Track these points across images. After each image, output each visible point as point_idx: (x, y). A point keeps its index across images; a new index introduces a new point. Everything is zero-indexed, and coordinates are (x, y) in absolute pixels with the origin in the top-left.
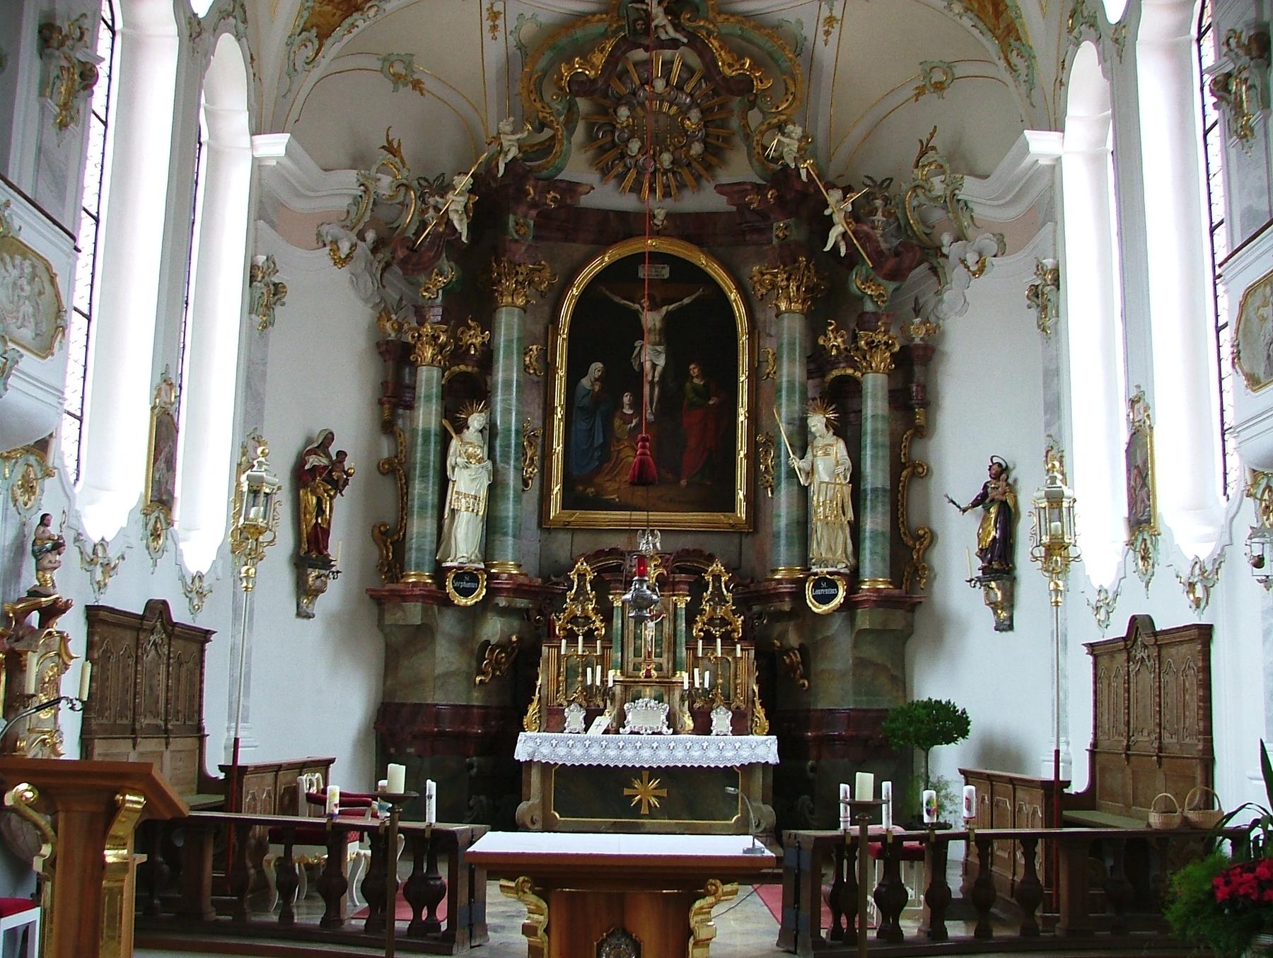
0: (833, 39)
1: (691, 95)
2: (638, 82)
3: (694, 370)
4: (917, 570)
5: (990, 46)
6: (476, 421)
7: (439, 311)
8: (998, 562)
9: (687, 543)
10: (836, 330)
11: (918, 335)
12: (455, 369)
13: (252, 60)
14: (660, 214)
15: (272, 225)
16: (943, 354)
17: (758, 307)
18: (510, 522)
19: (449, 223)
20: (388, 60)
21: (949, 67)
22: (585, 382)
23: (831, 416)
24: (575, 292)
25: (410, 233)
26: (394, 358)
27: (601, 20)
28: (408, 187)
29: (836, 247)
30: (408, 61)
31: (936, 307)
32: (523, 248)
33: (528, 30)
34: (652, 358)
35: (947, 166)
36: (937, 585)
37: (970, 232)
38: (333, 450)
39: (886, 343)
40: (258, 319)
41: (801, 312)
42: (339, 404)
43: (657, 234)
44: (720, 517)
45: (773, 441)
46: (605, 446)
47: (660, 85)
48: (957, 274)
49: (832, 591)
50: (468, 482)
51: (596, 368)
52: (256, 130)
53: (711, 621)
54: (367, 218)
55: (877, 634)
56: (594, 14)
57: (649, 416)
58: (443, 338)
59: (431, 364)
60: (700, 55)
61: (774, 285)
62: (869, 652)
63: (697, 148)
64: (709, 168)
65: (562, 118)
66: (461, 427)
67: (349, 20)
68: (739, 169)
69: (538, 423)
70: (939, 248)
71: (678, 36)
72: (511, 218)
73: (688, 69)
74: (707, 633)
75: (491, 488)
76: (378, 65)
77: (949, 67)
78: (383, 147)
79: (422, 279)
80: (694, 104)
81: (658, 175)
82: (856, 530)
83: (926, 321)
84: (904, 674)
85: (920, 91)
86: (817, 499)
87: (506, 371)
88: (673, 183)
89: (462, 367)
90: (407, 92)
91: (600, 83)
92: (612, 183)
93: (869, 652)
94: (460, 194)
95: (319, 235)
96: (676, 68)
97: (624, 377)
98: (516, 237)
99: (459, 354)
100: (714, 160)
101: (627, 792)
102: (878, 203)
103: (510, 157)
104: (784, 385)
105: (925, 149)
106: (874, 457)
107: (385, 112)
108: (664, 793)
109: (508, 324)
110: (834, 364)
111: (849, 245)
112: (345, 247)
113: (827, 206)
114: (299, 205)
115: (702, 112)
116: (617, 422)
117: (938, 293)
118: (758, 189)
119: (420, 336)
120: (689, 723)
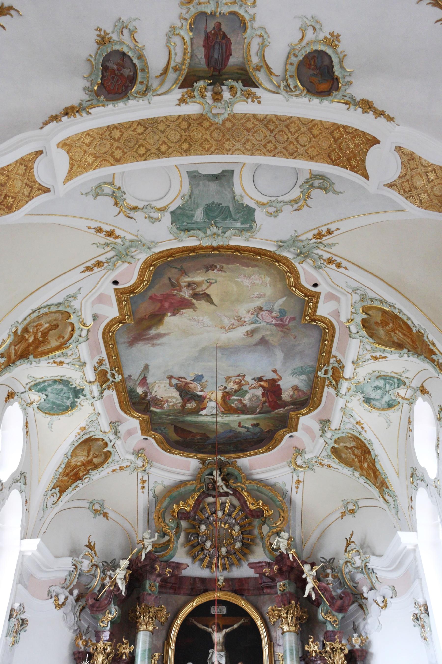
0: (300, 490)
1: (235, 519)
2: (210, 513)
5: (375, 492)
10: (314, 642)
11: (357, 643)
14: (221, 579)
15: (25, 586)
16: (372, 654)
17: (272, 629)
19: (116, 585)
20: (92, 503)
21: (356, 503)
24: (179, 622)
25: (96, 591)
27: (193, 484)
31: (364, 626)
32: (153, 598)
33: (159, 489)
35: (361, 551)
37: (377, 585)
39: (341, 648)
40: (10, 640)
41: (295, 632)
43: (220, 590)
47: (220, 514)
48: (373, 609)
54: (75, 583)
56: (189, 481)
58: (109, 650)
60: (239, 500)
61: (280, 617)
63: (238, 545)
64: (245, 555)
65: (174, 531)
67: (75, 484)
68: (259, 555)
70: (362, 594)
71: (228, 491)
72: (148, 583)
73: (234, 507)
76: (87, 505)
77: (356, 503)
78: (86, 546)
80: (236, 523)
81: (220, 559)
85: (343, 514)
88: (227, 563)
91: (192, 513)
92: (197, 563)
94: (123, 570)
95: (49, 592)
96: (228, 505)
98: (150, 592)
100: (246, 551)
102: (329, 571)
103: (148, 550)
107: (90, 529)
109: (143, 640)
111: (317, 594)
112: (62, 599)
113: (303, 573)
114: (41, 576)
115: (240, 527)
117: (364, 619)
118: (269, 565)
119: (97, 648)
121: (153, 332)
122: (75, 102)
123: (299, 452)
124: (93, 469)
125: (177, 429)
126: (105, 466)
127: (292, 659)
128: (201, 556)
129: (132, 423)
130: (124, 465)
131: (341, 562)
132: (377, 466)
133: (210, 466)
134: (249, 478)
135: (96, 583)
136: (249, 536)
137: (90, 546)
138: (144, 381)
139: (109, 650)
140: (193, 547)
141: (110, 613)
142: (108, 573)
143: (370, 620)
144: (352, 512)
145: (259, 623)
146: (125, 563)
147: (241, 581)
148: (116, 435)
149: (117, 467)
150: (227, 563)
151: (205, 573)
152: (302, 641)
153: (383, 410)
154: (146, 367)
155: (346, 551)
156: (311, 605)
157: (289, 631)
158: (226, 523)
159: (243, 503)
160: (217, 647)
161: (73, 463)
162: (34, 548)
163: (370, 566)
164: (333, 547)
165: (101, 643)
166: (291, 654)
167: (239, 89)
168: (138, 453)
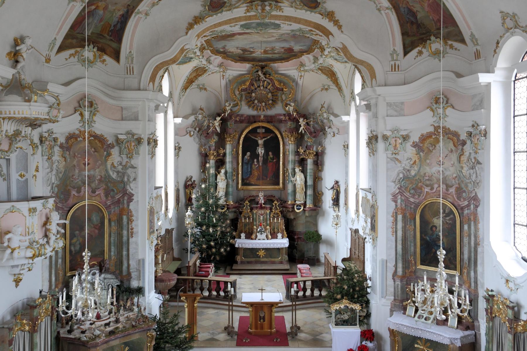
3: (270, 153)
5: (337, 89)
6: (223, 171)
8: (336, 202)
9: (269, 193)
13: (173, 105)
14: (262, 116)
19: (216, 129)
21: (329, 86)
22: (246, 157)
24: (243, 136)
25: (206, 128)
26: (204, 157)
28: (205, 117)
29: (302, 131)
30: (203, 85)
33: (231, 77)
34: (261, 151)
36: (323, 204)
37: (332, 126)
38: (192, 180)
40: (176, 157)
42: (193, 170)
44: (277, 187)
45: (287, 169)
46: (251, 171)
48: (329, 136)
50: (222, 185)
51: (248, 154)
52: (174, 117)
53: (274, 213)
55: (310, 216)
57: (260, 164)
62: (309, 219)
63: (270, 102)
69: (236, 166)
70: (325, 129)
72: (229, 123)
75: (227, 185)
77: (329, 86)
82: (306, 193)
83: (322, 146)
85: (322, 90)
87: (228, 159)
90: (203, 91)
93: (309, 219)
99: (218, 155)
100: (274, 103)
105: (322, 107)
109: (228, 148)
110: (301, 155)
112: (192, 133)
116: (253, 166)
118: (284, 115)
120: (270, 237)
121: (229, 39)
122: (197, 14)
123: (302, 65)
128: (253, 105)
131: (318, 115)
134: (276, 72)
136: (276, 97)
137: (201, 109)
140: (249, 102)
142: (211, 121)
144: (327, 89)
145: (279, 136)
146: (218, 119)
147: (271, 117)
150: (265, 109)
152: (297, 146)
154: (226, 46)
156: (302, 136)
159: (273, 85)
161: (190, 78)
164: (315, 104)
168: (220, 65)
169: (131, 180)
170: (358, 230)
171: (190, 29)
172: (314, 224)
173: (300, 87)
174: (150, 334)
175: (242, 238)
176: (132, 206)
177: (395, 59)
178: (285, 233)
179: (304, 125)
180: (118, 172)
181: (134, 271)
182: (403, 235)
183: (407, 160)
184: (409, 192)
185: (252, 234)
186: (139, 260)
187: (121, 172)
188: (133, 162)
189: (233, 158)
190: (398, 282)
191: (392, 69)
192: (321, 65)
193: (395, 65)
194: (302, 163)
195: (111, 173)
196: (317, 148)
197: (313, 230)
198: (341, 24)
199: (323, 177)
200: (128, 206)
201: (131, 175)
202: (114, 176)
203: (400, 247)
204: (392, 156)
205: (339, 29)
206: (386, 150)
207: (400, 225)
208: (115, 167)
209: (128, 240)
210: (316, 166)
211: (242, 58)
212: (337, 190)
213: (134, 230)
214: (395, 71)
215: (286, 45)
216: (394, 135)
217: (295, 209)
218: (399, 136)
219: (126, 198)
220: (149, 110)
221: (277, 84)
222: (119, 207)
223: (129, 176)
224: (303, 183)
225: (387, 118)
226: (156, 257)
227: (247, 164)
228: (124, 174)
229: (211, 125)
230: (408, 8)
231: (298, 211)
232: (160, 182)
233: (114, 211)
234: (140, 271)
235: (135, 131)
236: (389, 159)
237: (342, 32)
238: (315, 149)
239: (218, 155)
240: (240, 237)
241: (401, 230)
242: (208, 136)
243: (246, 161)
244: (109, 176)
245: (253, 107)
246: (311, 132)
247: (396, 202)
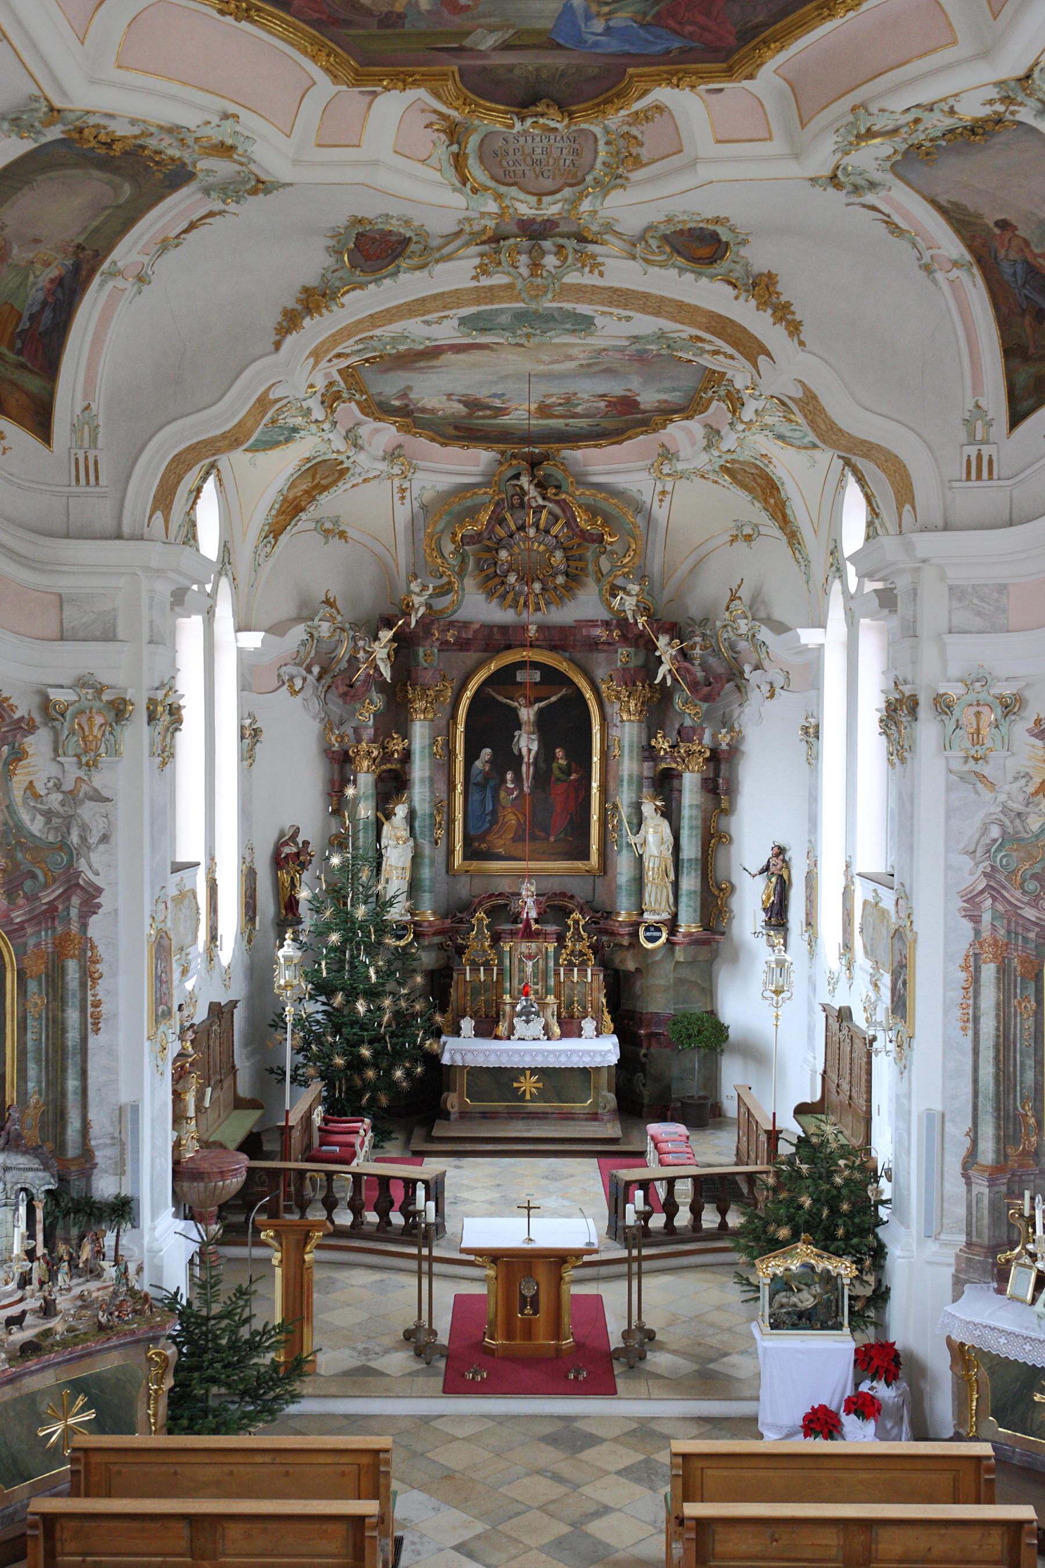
0: (666, 504)
2: (514, 528)
3: (559, 752)
4: (720, 912)
6: (401, 811)
7: (371, 731)
8: (777, 915)
9: (555, 885)
10: (664, 737)
11: (724, 740)
12: (384, 767)
16: (743, 753)
18: (427, 882)
19: (377, 668)
22: (478, 764)
23: (658, 803)
24: (469, 694)
25: (344, 665)
26: (340, 764)
29: (664, 678)
30: (336, 521)
33: (428, 496)
34: (527, 744)
35: (749, 615)
36: (735, 923)
37: (766, 663)
38: (300, 840)
41: (639, 721)
42: (304, 811)
44: (579, 864)
45: (615, 807)
46: (494, 812)
48: (756, 696)
49: (658, 934)
50: (397, 856)
51: (486, 753)
52: (238, 629)
54: (312, 655)
55: (691, 963)
59: (368, 772)
60: (563, 510)
62: (686, 973)
63: (560, 580)
66: (389, 815)
71: (546, 503)
72: (421, 650)
74: (570, 961)
77: (756, 526)
79: (358, 706)
82: (676, 885)
83: (731, 729)
84: (711, 985)
85: (734, 539)
86: (649, 864)
87: (419, 770)
89: (389, 766)
92: (495, 601)
93: (686, 973)
94: (385, 647)
95: (279, 676)
97: (508, 760)
98: (425, 665)
99: (387, 757)
100: (572, 584)
101: (515, 1085)
102: (698, 639)
103: (420, 614)
104: (626, 778)
106: (690, 836)
108: (540, 1085)
109: (420, 733)
110: (663, 759)
111: (675, 680)
112: (298, 683)
113: (656, 648)
116: (502, 794)
118: (607, 624)
120: (557, 1030)
121: (422, 364)
123: (667, 455)
124: (320, 493)
125: (456, 428)
126: (340, 484)
127: (631, 759)
129: (384, 434)
130: (371, 476)
131: (718, 624)
132: (788, 512)
133: (514, 462)
134: (581, 480)
135: (343, 651)
137: (327, 602)
138: (404, 395)
139: (375, 753)
140: (488, 578)
141: (371, 703)
143: (747, 710)
144: (748, 538)
145: (589, 695)
148: (355, 446)
149: (360, 480)
150: (542, 603)
151: (506, 616)
153: (806, 448)
154: (410, 388)
155: (727, 609)
157: (629, 721)
158: (540, 544)
159: (571, 522)
160: (525, 728)
161: (291, 496)
162: (259, 645)
163: (758, 636)
164: (709, 590)
165: (364, 744)
166: (631, 751)
167: (570, 250)
168: (393, 455)
169: (93, 840)
170: (849, 1009)
171: (289, 331)
172: (703, 989)
173: (660, 536)
174: (158, 1354)
175: (463, 1033)
176: (96, 927)
177: (979, 437)
178: (607, 1017)
179: (673, 658)
180: (49, 815)
181: (105, 1145)
182: (997, 1029)
183: (1016, 779)
184: (1022, 888)
185: (496, 1021)
186: (120, 1108)
187: (57, 815)
188: (98, 780)
189: (435, 766)
190: (982, 1187)
191: (969, 473)
192: (729, 457)
193: (979, 457)
194: (664, 784)
195: (25, 817)
196: (714, 736)
197: (698, 1007)
198: (798, 317)
199: (733, 833)
200: (84, 926)
201: (92, 824)
202: (36, 826)
203: (987, 1070)
204: (966, 768)
205: (791, 334)
206: (947, 745)
207: (989, 997)
208: (37, 797)
209: (84, 1040)
210: (710, 796)
211: (466, 429)
212: (781, 876)
213: (103, 1009)
214: (979, 477)
215: (616, 388)
216: (972, 697)
217: (642, 939)
218: (990, 699)
219: (75, 901)
220: (151, 607)
221: (581, 519)
222: (54, 929)
223: (84, 828)
224: (668, 854)
225: (949, 639)
226: (177, 1096)
227: (482, 786)
228: (68, 821)
229: (361, 655)
230: (1026, 262)
231: (649, 946)
232: (189, 846)
233: (37, 945)
234: (123, 1144)
235: (104, 677)
236: (953, 778)
237: (802, 343)
238: (707, 739)
239: (387, 757)
240: (457, 1032)
241: (993, 1013)
242: (351, 693)
243: (479, 778)
244: (19, 826)
245: (503, 597)
246: (693, 680)
247: (976, 919)
